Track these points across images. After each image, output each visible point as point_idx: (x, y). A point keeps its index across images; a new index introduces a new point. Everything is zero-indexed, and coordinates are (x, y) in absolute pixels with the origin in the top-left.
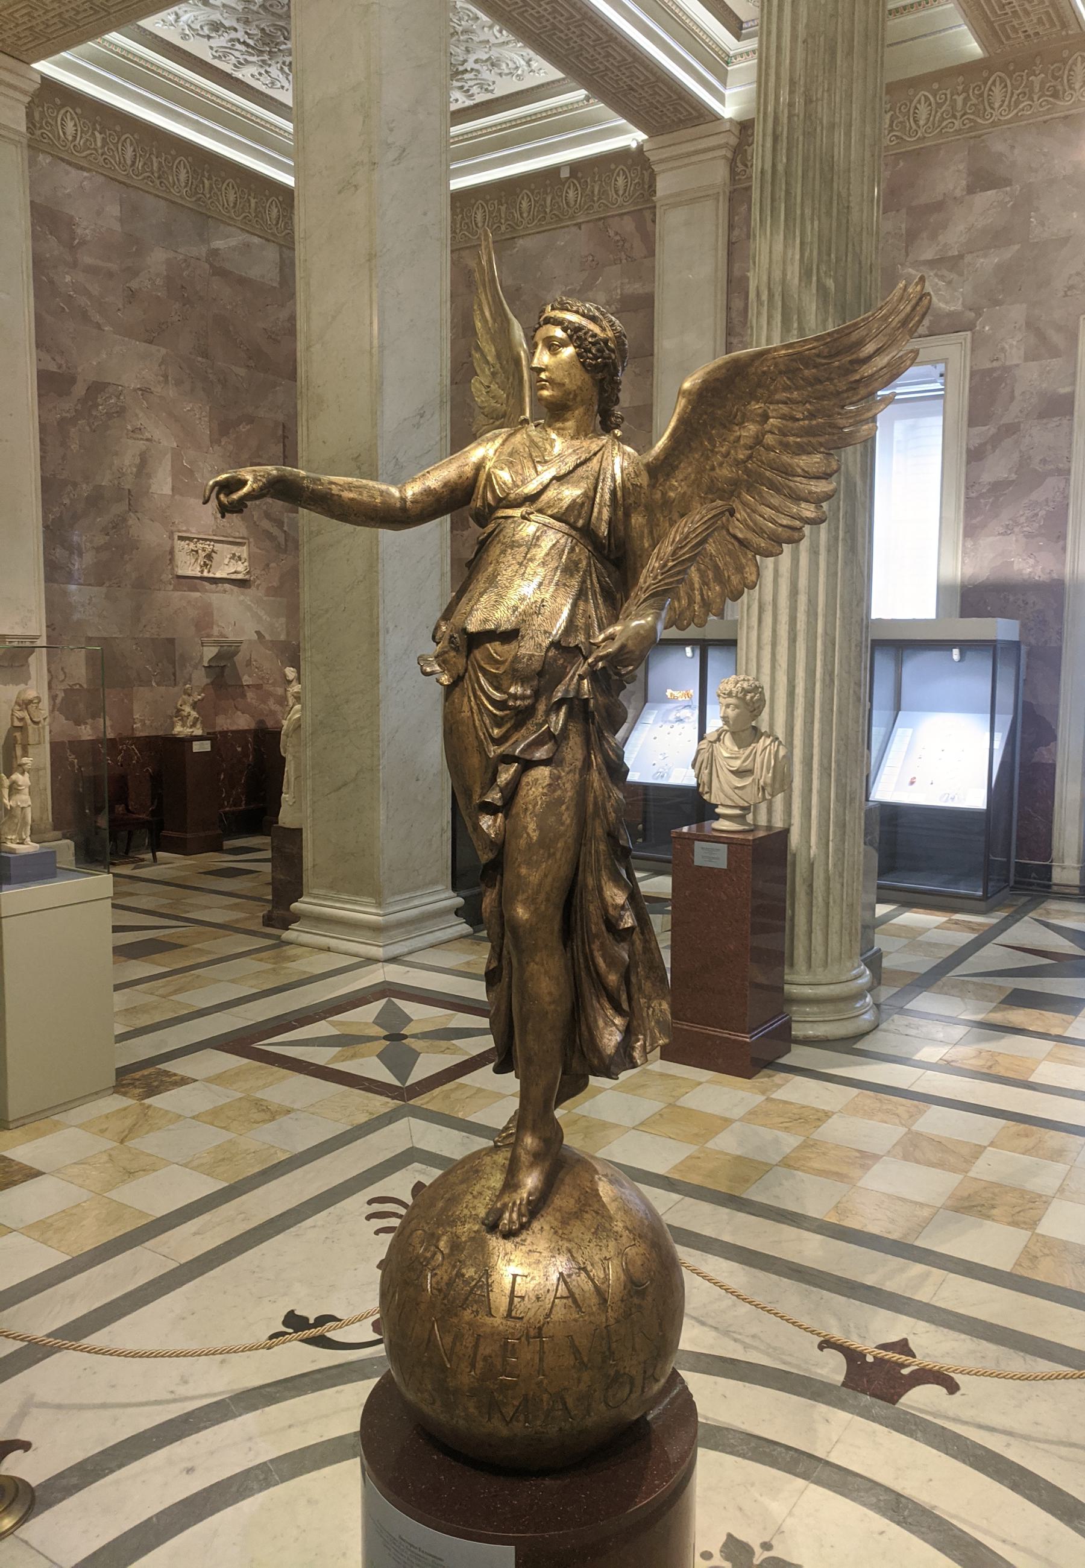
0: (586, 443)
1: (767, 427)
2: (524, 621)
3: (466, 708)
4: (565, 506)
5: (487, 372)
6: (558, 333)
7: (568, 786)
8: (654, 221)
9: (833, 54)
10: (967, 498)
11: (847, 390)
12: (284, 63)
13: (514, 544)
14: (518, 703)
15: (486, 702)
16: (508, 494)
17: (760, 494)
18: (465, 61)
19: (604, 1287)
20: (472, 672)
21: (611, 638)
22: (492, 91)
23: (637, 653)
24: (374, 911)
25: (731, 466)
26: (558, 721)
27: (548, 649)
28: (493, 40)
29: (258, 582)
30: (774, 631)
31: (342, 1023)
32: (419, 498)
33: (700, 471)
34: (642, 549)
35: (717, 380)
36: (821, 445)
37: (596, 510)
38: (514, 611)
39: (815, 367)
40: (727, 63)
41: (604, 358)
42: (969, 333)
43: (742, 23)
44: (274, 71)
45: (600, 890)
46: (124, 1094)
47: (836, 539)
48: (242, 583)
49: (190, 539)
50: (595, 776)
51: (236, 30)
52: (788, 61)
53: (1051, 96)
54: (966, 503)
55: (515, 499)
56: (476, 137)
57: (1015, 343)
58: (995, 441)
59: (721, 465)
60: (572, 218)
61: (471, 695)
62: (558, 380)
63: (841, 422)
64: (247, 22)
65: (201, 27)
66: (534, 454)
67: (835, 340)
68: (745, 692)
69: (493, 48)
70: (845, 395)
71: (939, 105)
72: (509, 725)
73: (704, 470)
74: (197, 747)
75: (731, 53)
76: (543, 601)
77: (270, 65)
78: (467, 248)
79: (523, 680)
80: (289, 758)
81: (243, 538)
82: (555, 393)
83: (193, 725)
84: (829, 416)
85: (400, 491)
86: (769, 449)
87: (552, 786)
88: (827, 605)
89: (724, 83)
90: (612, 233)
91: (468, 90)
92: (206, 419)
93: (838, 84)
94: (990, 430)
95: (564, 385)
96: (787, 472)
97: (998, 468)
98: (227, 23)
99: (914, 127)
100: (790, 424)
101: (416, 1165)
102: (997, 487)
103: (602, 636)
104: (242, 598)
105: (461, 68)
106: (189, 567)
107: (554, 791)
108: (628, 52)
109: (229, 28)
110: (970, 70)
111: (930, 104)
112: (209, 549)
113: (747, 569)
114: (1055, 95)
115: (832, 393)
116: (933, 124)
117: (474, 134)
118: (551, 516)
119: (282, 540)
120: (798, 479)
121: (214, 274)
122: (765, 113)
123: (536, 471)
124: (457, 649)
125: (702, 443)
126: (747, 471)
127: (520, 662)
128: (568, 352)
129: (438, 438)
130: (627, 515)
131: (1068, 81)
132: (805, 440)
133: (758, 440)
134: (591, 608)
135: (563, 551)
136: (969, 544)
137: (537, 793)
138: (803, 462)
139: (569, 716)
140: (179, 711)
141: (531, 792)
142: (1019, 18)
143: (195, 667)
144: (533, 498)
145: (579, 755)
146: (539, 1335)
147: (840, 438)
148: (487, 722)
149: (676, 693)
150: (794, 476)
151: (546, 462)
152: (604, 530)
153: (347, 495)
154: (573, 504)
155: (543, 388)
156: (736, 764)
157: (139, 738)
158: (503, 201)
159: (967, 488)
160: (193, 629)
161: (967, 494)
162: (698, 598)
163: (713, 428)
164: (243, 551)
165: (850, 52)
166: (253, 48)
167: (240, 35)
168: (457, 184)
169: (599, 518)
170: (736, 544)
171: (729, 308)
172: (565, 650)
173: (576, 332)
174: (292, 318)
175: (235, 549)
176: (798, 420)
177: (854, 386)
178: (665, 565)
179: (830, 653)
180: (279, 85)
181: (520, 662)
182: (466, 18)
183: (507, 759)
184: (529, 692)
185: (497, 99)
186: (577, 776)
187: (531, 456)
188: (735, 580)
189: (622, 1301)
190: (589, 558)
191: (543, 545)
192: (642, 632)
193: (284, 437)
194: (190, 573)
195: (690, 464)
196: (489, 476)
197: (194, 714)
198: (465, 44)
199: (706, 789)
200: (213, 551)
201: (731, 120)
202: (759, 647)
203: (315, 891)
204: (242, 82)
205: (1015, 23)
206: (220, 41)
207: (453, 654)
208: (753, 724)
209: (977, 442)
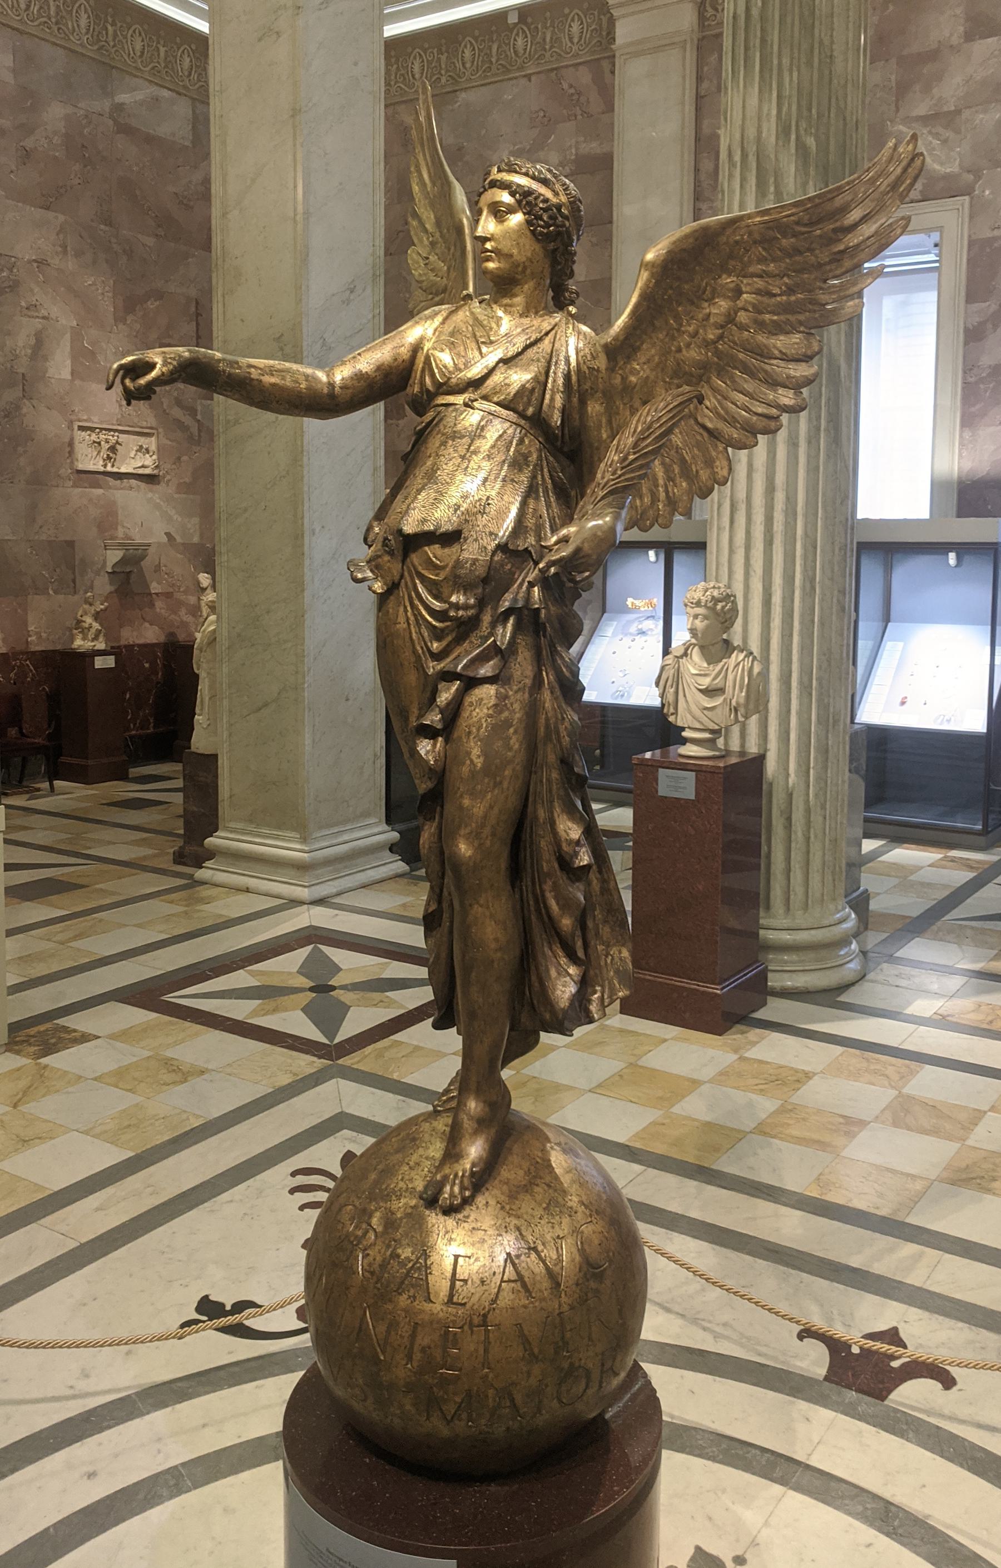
0: (536, 322)
1: (740, 303)
3: (401, 619)
4: (513, 392)
6: (505, 197)
7: (517, 706)
8: (613, 72)
11: (830, 262)
13: (456, 435)
14: (461, 613)
15: (424, 612)
16: (449, 379)
17: (732, 378)
19: (556, 1269)
20: (408, 579)
21: (565, 540)
23: (594, 557)
24: (298, 846)
25: (699, 347)
26: (505, 633)
27: (494, 553)
29: (168, 477)
30: (748, 533)
31: (262, 973)
32: (349, 383)
33: (665, 353)
36: (801, 323)
37: (548, 396)
38: (456, 510)
39: (794, 236)
41: (557, 226)
42: (967, 198)
45: (553, 823)
46: (18, 1052)
48: (151, 479)
49: (92, 429)
50: (546, 695)
54: (963, 388)
55: (457, 385)
59: (688, 346)
60: (521, 68)
61: (407, 604)
62: (506, 251)
63: (823, 298)
66: (478, 334)
68: (716, 600)
70: (828, 268)
73: (669, 352)
74: (99, 663)
76: (488, 498)
79: (467, 588)
80: (203, 675)
82: (502, 265)
83: (95, 638)
84: (810, 291)
85: (328, 376)
86: (742, 328)
87: (499, 707)
88: (807, 503)
90: (565, 86)
92: (110, 294)
95: (511, 256)
96: (763, 354)
100: (765, 300)
101: (345, 1132)
103: (554, 539)
104: (150, 495)
106: (90, 461)
107: (501, 712)
112: (113, 440)
113: (718, 463)
119: (195, 430)
120: (775, 362)
121: (118, 132)
123: (481, 353)
124: (391, 553)
125: (667, 322)
126: (717, 353)
127: (462, 567)
128: (517, 219)
129: (370, 316)
130: (583, 403)
132: (782, 317)
133: (730, 318)
134: (543, 507)
135: (511, 442)
136: (967, 434)
137: (481, 715)
138: (781, 342)
139: (517, 628)
140: (79, 622)
143: (98, 573)
144: (476, 384)
145: (529, 671)
146: (484, 1323)
147: (822, 316)
149: (637, 602)
150: (771, 358)
151: (492, 342)
152: (556, 419)
153: (268, 379)
154: (522, 391)
155: (488, 259)
156: (705, 682)
157: (34, 653)
158: (444, 49)
160: (95, 530)
161: (964, 378)
162: (662, 495)
163: (679, 304)
164: (152, 443)
169: (552, 406)
170: (705, 434)
171: (697, 170)
172: (512, 553)
173: (525, 197)
175: (142, 441)
176: (775, 295)
177: (838, 258)
178: (625, 458)
181: (462, 567)
183: (448, 676)
184: (472, 601)
186: (527, 695)
187: (475, 336)
188: (704, 475)
189: (577, 1285)
190: (540, 451)
191: (488, 435)
192: (599, 533)
193: (198, 315)
194: (91, 467)
195: (654, 345)
196: (427, 359)
197: (96, 626)
199: (672, 710)
200: (117, 442)
203: (232, 825)
207: (387, 558)
208: (725, 636)
209: (976, 320)
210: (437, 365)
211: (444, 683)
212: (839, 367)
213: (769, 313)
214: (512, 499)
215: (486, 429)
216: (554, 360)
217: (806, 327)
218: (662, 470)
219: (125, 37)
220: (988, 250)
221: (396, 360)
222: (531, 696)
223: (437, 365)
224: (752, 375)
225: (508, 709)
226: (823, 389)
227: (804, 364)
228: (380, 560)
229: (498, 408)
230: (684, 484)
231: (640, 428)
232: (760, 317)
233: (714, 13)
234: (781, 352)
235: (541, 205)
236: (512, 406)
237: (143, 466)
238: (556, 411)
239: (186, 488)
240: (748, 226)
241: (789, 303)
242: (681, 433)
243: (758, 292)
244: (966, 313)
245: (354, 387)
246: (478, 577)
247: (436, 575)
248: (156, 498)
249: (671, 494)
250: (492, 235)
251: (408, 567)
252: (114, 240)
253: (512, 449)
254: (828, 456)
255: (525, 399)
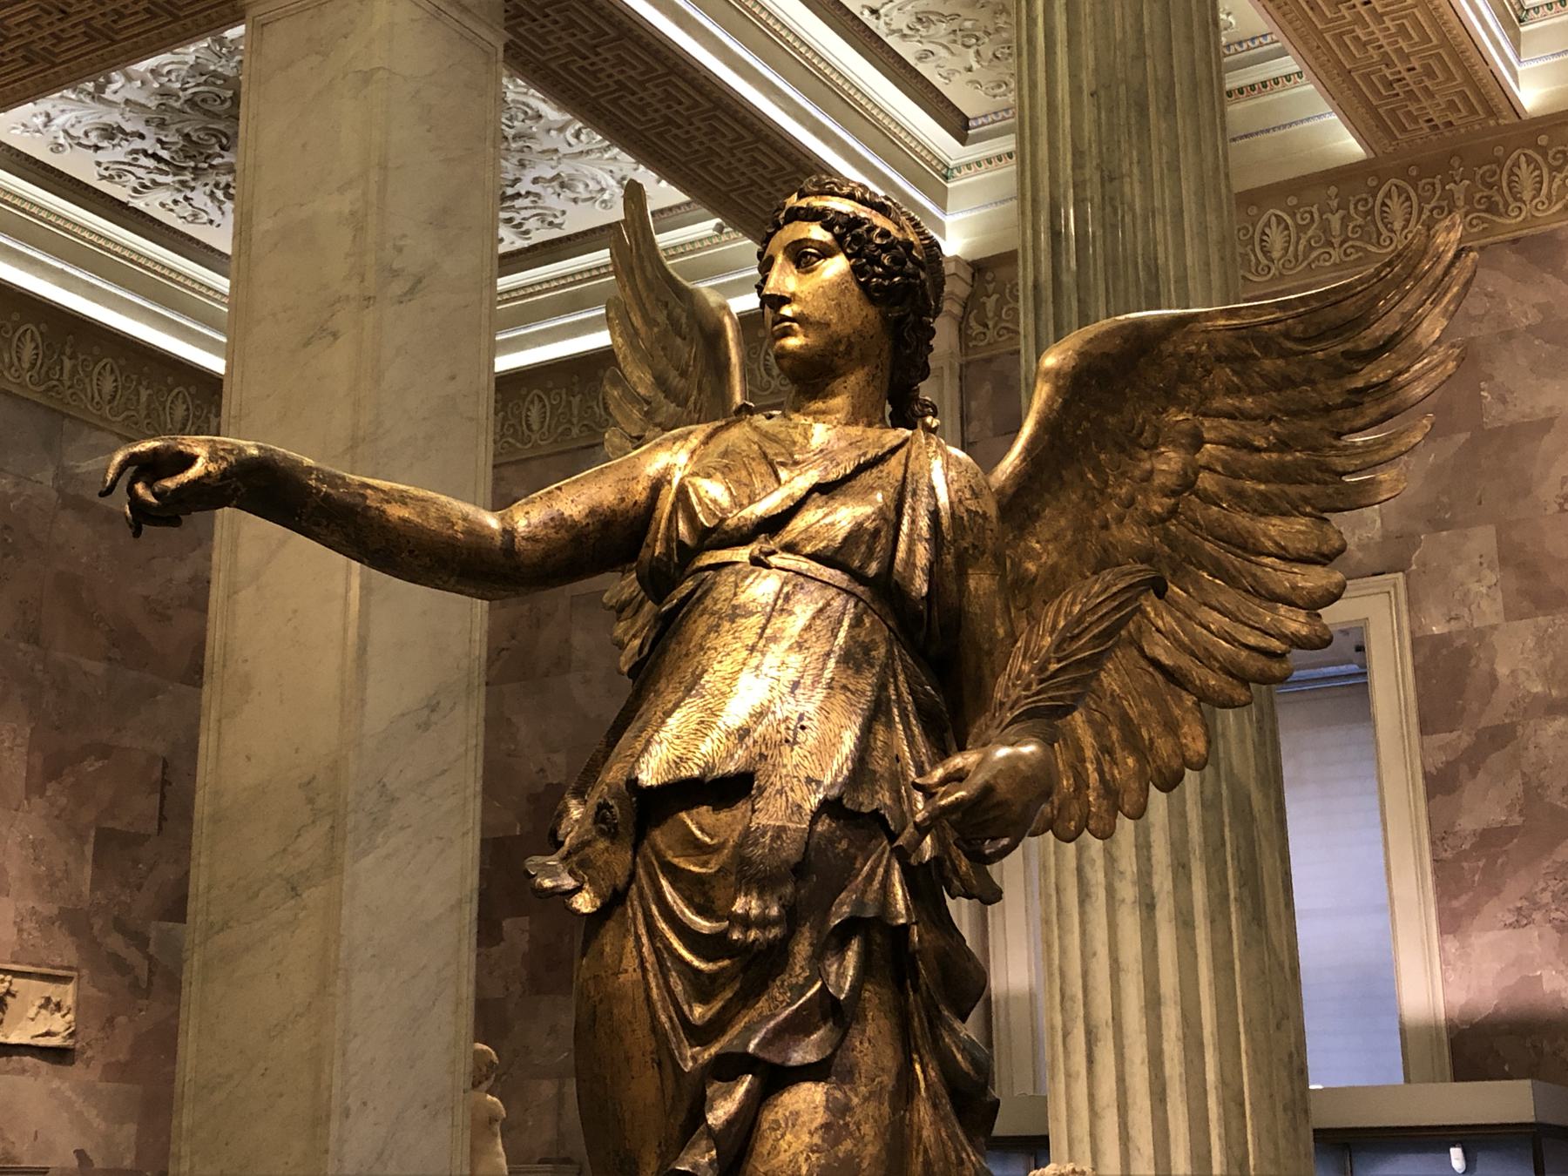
0: (873, 433)
1: (1201, 458)
2: (763, 757)
3: (630, 962)
4: (840, 539)
5: (636, 415)
6: (816, 232)
7: (867, 1129)
9: (1143, 110)
10: (1436, 860)
11: (1342, 406)
12: (217, 185)
13: (737, 613)
14: (753, 934)
15: (676, 944)
16: (722, 520)
17: (1197, 582)
18: (517, 180)
20: (645, 881)
21: (958, 777)
22: (559, 226)
23: (1017, 808)
25: (1138, 524)
26: (844, 971)
27: (816, 816)
28: (564, 149)
29: (89, 1053)
30: (1121, 1080)
32: (541, 533)
33: (1082, 527)
34: (992, 638)
35: (1106, 355)
36: (1306, 500)
37: (902, 546)
38: (741, 738)
39: (1280, 356)
40: (946, 178)
41: (905, 275)
42: (1400, 575)
43: (967, 119)
44: (200, 198)
47: (1225, 897)
48: (58, 1056)
50: (923, 1112)
51: (142, 137)
52: (1068, 122)
53: (1486, 211)
54: (1435, 872)
55: (738, 528)
56: (531, 295)
57: (1484, 590)
58: (1473, 759)
59: (1120, 520)
61: (642, 931)
62: (817, 315)
63: (1339, 463)
64: (162, 125)
65: (86, 134)
66: (770, 452)
67: (1314, 311)
69: (565, 160)
70: (1340, 414)
71: (1301, 229)
72: (729, 994)
73: (1090, 527)
75: (952, 164)
76: (801, 718)
77: (193, 189)
78: (513, 463)
79: (762, 883)
81: (70, 968)
82: (809, 341)
84: (1315, 449)
85: (502, 519)
86: (1208, 499)
87: (833, 1130)
88: (1220, 1026)
89: (943, 206)
91: (520, 225)
92: (24, 750)
93: (1155, 155)
94: (1461, 738)
95: (828, 325)
96: (1247, 546)
97: (1484, 807)
98: (128, 127)
99: (1264, 261)
100: (1244, 455)
102: (1489, 839)
103: (939, 773)
104: (55, 1084)
105: (510, 191)
107: (837, 1141)
108: (787, 157)
109: (133, 134)
110: (1345, 175)
111: (1287, 227)
113: (1186, 729)
114: (1492, 208)
115: (1315, 408)
116: (1296, 256)
117: (530, 290)
118: (812, 557)
119: (143, 974)
120: (1268, 560)
121: (64, 507)
122: (1035, 201)
123: (778, 480)
124: (612, 834)
125: (1082, 476)
126: (1168, 539)
127: (756, 843)
128: (837, 266)
129: (463, 748)
130: (962, 575)
131: (1510, 189)
132: (1274, 488)
133: (1186, 483)
134: (902, 741)
135: (840, 622)
136: (1452, 945)
137: (796, 1147)
138: (1275, 529)
139: (866, 970)
141: (783, 1144)
142: (1418, 100)
144: (774, 524)
145: (889, 1059)
147: (1338, 492)
148: (679, 989)
150: (1260, 554)
151: (796, 463)
152: (920, 585)
153: (396, 511)
154: (855, 535)
155: (787, 333)
158: (576, 389)
159: (1433, 843)
161: (1434, 852)
162: (1094, 777)
163: (1102, 449)
164: (66, 994)
165: (1169, 109)
166: (167, 163)
167: (149, 145)
168: (505, 363)
169: (910, 563)
170: (1159, 677)
172: (849, 815)
173: (850, 230)
174: (201, 584)
175: (51, 990)
176: (1258, 450)
177: (1356, 399)
178: (1042, 668)
179: (1234, 1124)
180: (205, 218)
181: (756, 843)
182: (521, 116)
183: (728, 1068)
184: (774, 911)
185: (568, 238)
186: (886, 1109)
187: (765, 455)
188: (1164, 746)
190: (889, 642)
191: (797, 609)
192: (1022, 766)
193: (165, 782)
195: (1063, 512)
196: (682, 492)
198: (519, 156)
200: (8, 992)
201: (956, 259)
202: (1094, 1115)
204: (144, 215)
205: (1413, 107)
206: (115, 153)
207: (602, 844)
209: (1441, 759)
210: (700, 499)
211: (717, 1085)
212: (1249, 797)
213: (1252, 478)
214: (844, 721)
215: (794, 599)
216: (909, 488)
217: (1314, 507)
218: (1089, 732)
219: (89, 375)
220: (1444, 652)
221: (623, 500)
222: (894, 1110)
223: (700, 499)
224: (1232, 580)
225: (851, 1134)
226: (1227, 830)
227: (1319, 569)
228: (588, 850)
229: (814, 565)
230: (1130, 761)
231: (1062, 623)
232: (1237, 484)
233: (981, 329)
234: (1277, 544)
235: (878, 241)
236: (839, 558)
237: (48, 1034)
238: (918, 572)
239: (118, 1071)
240: (1206, 331)
241: (1283, 465)
242: (1117, 670)
243: (1231, 443)
244: (1422, 747)
245: (548, 540)
246: (787, 861)
247: (704, 865)
248: (66, 1088)
249: (1108, 777)
250: (794, 294)
251: (645, 857)
252: (39, 667)
253: (842, 634)
254: (1246, 945)
255: (863, 548)
